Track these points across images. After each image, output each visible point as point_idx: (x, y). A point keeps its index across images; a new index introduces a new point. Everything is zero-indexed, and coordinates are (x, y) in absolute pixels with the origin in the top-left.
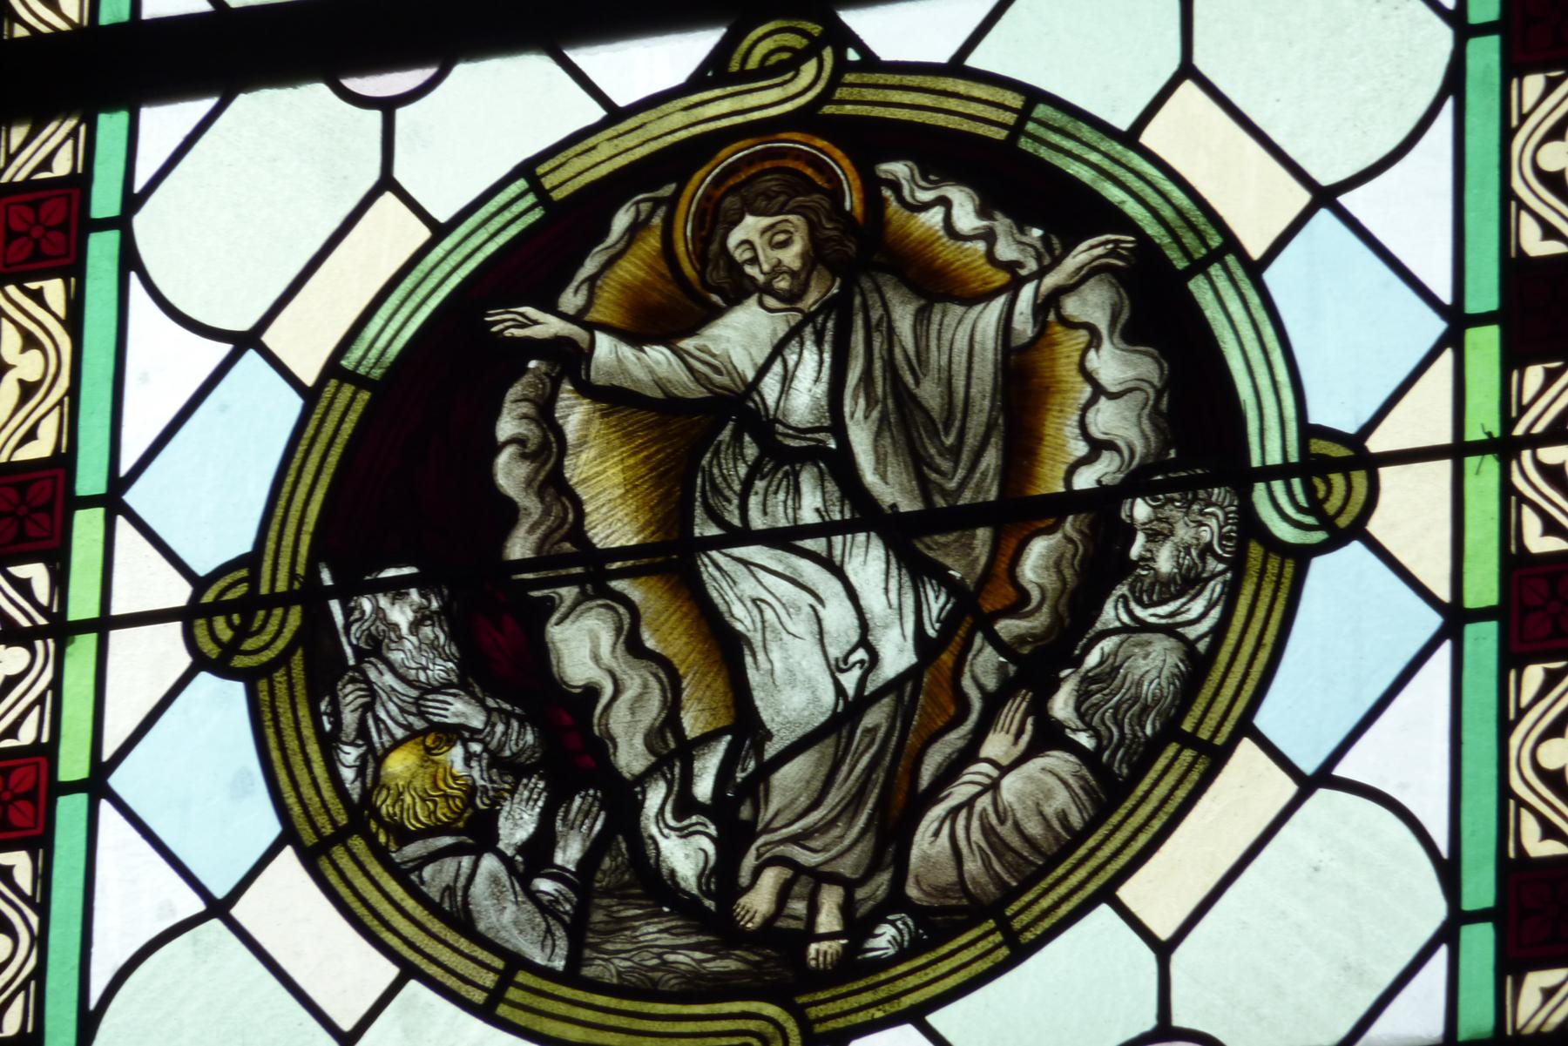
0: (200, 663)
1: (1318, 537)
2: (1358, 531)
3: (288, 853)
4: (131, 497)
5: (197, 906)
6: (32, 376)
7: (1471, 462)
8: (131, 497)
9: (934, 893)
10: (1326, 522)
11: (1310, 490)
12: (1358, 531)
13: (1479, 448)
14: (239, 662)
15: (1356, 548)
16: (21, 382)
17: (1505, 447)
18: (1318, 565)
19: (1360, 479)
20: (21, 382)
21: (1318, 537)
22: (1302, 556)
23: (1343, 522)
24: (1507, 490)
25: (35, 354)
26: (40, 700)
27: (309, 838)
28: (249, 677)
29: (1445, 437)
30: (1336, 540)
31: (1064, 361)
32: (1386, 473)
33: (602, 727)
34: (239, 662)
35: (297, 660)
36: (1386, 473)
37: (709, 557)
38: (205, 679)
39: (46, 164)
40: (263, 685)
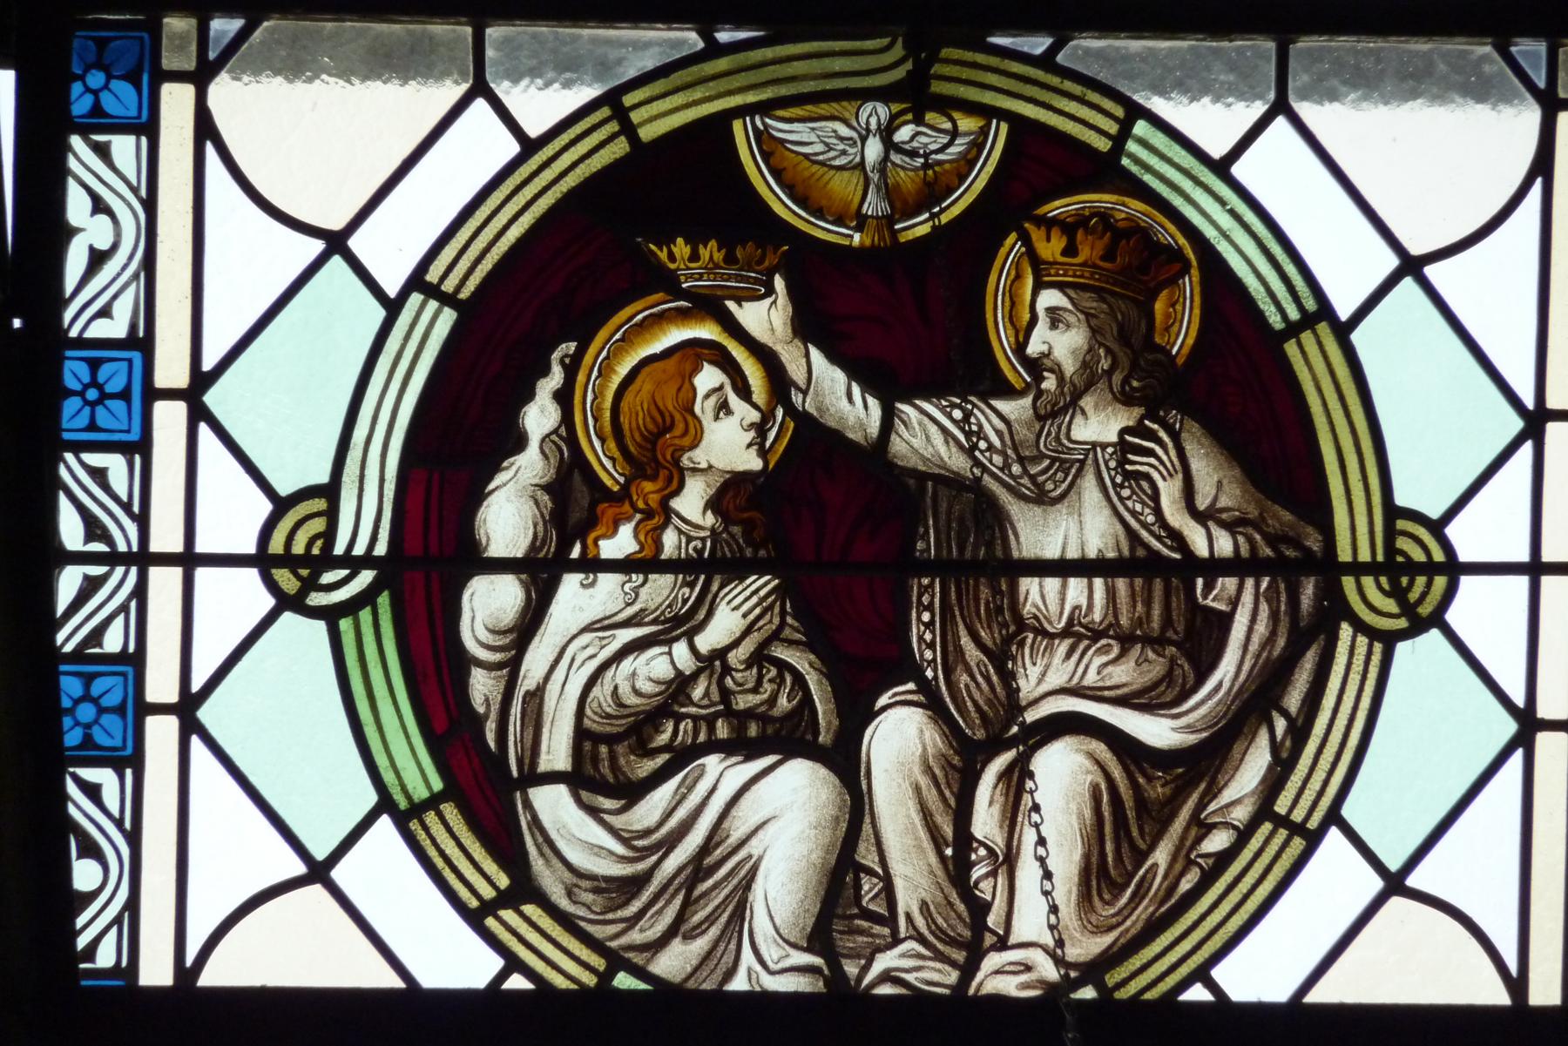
0: (1437, 527)
1: (1402, 623)
2: (1437, 620)
3: (1344, 313)
4: (211, 398)
5: (1430, 271)
6: (103, 244)
7: (176, 545)
8: (211, 398)
9: (1038, 985)
10: (1408, 609)
11: (1394, 582)
12: (1437, 620)
13: (166, 559)
14: (316, 599)
15: (1435, 634)
16: (92, 249)
17: (144, 559)
18: (1402, 649)
19: (276, 545)
20: (92, 249)
21: (1402, 623)
22: (1389, 640)
23: (1425, 610)
24: (143, 520)
25: (103, 219)
26: (124, 608)
27: (1323, 328)
28: (330, 615)
29: (202, 574)
30: (1417, 627)
31: (501, 691)
32: (251, 548)
33: (1102, 279)
34: (316, 599)
35: (384, 600)
36: (251, 548)
37: (63, 644)
38: (288, 617)
39: (97, 635)
40: (345, 624)
